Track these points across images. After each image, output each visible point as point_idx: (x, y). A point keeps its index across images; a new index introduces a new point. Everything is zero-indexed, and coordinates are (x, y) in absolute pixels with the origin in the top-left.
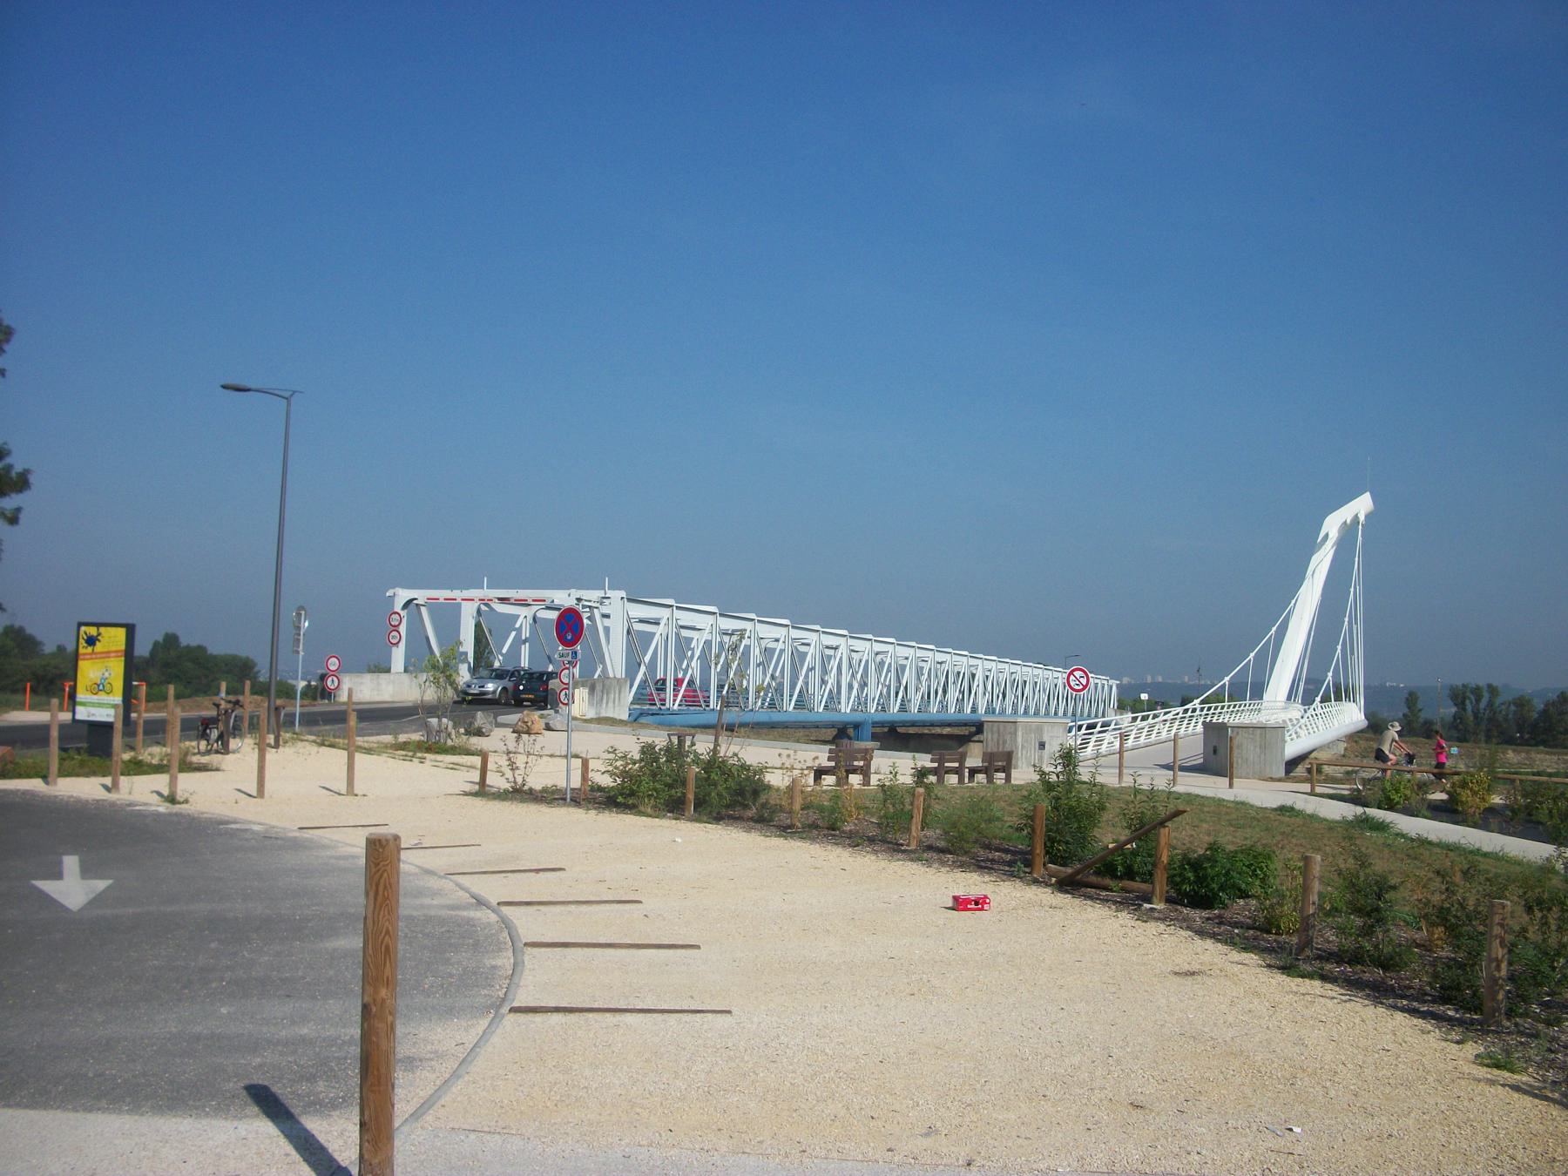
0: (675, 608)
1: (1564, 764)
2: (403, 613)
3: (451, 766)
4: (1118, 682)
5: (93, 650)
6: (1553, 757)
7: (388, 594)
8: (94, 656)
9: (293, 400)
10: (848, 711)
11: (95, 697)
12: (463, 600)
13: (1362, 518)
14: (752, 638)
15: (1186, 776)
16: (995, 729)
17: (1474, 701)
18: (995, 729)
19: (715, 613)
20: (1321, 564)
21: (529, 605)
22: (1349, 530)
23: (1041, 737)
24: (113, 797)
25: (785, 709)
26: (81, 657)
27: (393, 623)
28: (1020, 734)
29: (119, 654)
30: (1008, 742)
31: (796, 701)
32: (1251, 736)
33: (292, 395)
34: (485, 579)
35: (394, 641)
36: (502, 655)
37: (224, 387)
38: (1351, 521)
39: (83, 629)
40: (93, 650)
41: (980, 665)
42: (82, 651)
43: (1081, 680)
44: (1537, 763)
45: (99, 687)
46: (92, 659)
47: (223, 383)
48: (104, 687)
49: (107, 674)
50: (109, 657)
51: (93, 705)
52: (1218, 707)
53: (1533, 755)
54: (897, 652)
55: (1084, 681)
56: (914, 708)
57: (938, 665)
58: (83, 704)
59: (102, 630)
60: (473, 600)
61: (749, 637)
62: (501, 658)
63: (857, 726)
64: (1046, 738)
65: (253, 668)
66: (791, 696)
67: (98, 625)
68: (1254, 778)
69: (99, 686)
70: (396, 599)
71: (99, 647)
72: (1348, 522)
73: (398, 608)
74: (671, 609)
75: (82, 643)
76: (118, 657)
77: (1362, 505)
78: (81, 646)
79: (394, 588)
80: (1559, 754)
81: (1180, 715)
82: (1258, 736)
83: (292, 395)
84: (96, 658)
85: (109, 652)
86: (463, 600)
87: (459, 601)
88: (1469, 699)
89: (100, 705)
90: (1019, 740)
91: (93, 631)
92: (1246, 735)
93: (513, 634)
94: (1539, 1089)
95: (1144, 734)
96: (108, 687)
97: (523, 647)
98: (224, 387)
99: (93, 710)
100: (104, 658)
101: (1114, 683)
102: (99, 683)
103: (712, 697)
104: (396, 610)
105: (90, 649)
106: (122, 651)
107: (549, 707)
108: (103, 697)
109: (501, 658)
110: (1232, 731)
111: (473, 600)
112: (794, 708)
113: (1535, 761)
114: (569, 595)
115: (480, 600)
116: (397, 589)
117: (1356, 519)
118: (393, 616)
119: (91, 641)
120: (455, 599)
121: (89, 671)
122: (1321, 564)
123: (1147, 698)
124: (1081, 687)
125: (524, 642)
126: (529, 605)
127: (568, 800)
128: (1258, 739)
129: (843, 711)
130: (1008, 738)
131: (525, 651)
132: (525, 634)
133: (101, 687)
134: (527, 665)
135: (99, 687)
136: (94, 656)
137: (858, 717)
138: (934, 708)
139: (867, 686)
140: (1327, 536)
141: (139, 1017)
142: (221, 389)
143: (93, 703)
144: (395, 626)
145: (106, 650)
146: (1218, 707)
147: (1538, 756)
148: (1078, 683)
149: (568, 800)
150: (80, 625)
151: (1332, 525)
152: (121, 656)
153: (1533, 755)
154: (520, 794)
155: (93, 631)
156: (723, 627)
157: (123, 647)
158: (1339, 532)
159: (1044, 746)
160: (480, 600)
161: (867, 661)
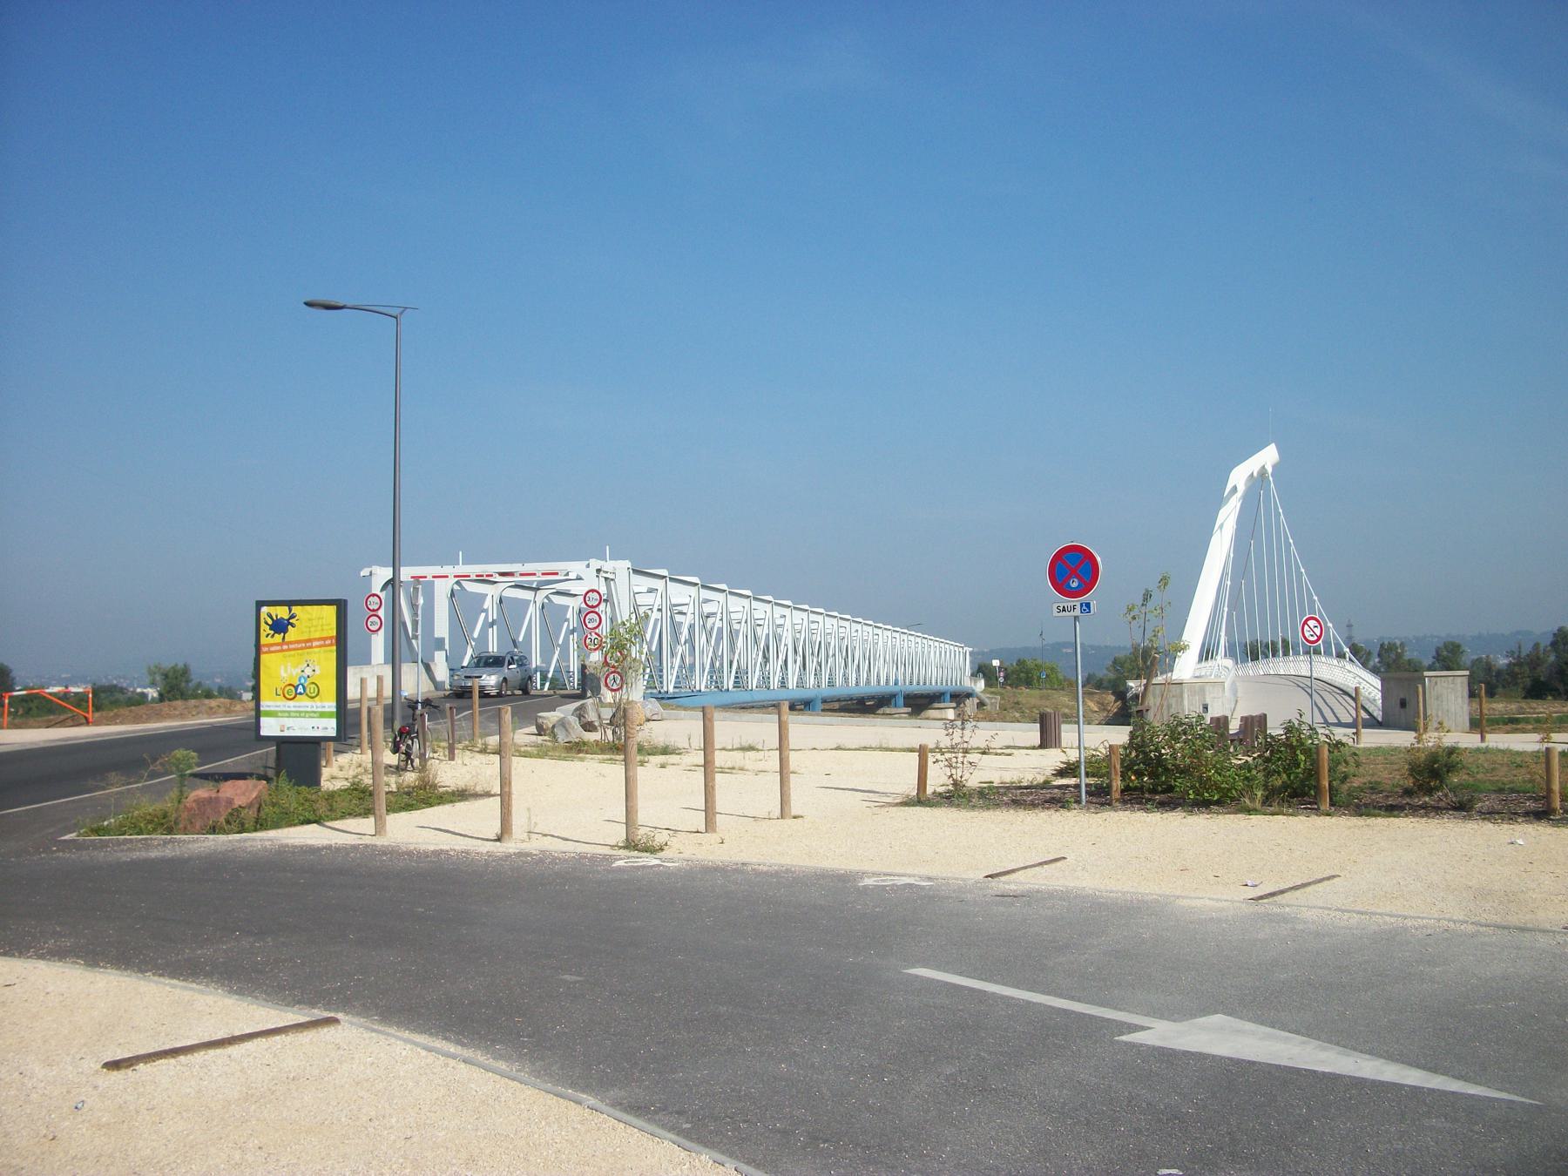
0: (668, 579)
2: (382, 595)
3: (693, 768)
4: (971, 649)
5: (284, 638)
7: (362, 574)
8: (285, 646)
9: (403, 319)
11: (291, 703)
12: (434, 577)
13: (1270, 470)
14: (664, 610)
15: (1381, 733)
16: (1158, 692)
18: (1158, 692)
19: (696, 584)
20: (1228, 516)
21: (496, 582)
22: (1258, 481)
23: (1204, 698)
24: (379, 841)
25: (750, 688)
26: (264, 649)
27: (371, 607)
28: (1186, 695)
29: (328, 642)
30: (1174, 706)
32: (1452, 686)
33: (401, 313)
34: (461, 553)
35: (372, 628)
36: (474, 639)
37: (308, 304)
38: (1258, 473)
39: (265, 610)
40: (284, 638)
41: (898, 637)
42: (264, 640)
43: (1315, 630)
45: (295, 690)
46: (282, 651)
47: (308, 299)
48: (304, 688)
49: (308, 671)
50: (311, 647)
51: (289, 714)
54: (828, 626)
55: (1318, 631)
58: (270, 714)
59: (296, 610)
60: (447, 577)
61: (660, 610)
62: (473, 644)
63: (943, 694)
64: (1208, 701)
65: (8, 675)
67: (290, 604)
68: (1457, 731)
69: (296, 688)
70: (373, 578)
71: (292, 634)
72: (1255, 474)
73: (376, 589)
75: (265, 629)
76: (325, 646)
77: (1268, 457)
78: (263, 635)
79: (371, 567)
82: (1459, 685)
83: (401, 313)
84: (289, 650)
85: (310, 640)
86: (434, 577)
87: (430, 578)
89: (300, 714)
90: (1186, 702)
91: (282, 612)
92: (1445, 685)
93: (483, 615)
96: (311, 689)
97: (490, 630)
98: (308, 304)
99: (288, 722)
100: (302, 648)
101: (969, 650)
102: (296, 683)
104: (374, 592)
105: (278, 638)
106: (331, 638)
107: (589, 694)
108: (303, 703)
109: (473, 644)
110: (1430, 681)
111: (447, 577)
114: (588, 566)
115: (455, 576)
116: (374, 567)
117: (1263, 471)
118: (371, 599)
119: (280, 627)
120: (425, 577)
121: (278, 668)
122: (1228, 516)
124: (1315, 638)
125: (492, 625)
126: (496, 582)
127: (1116, 795)
128: (1460, 689)
130: (1173, 701)
131: (493, 634)
132: (493, 615)
133: (300, 689)
134: (495, 650)
135: (295, 690)
136: (285, 647)
137: (896, 689)
140: (1235, 489)
141: (93, 1126)
142: (305, 306)
143: (289, 712)
144: (374, 610)
145: (305, 637)
148: (1312, 633)
149: (1116, 795)
150: (260, 604)
151: (1239, 476)
152: (331, 645)
154: (956, 796)
155: (282, 612)
157: (334, 633)
158: (1246, 484)
159: (1207, 708)
160: (455, 576)
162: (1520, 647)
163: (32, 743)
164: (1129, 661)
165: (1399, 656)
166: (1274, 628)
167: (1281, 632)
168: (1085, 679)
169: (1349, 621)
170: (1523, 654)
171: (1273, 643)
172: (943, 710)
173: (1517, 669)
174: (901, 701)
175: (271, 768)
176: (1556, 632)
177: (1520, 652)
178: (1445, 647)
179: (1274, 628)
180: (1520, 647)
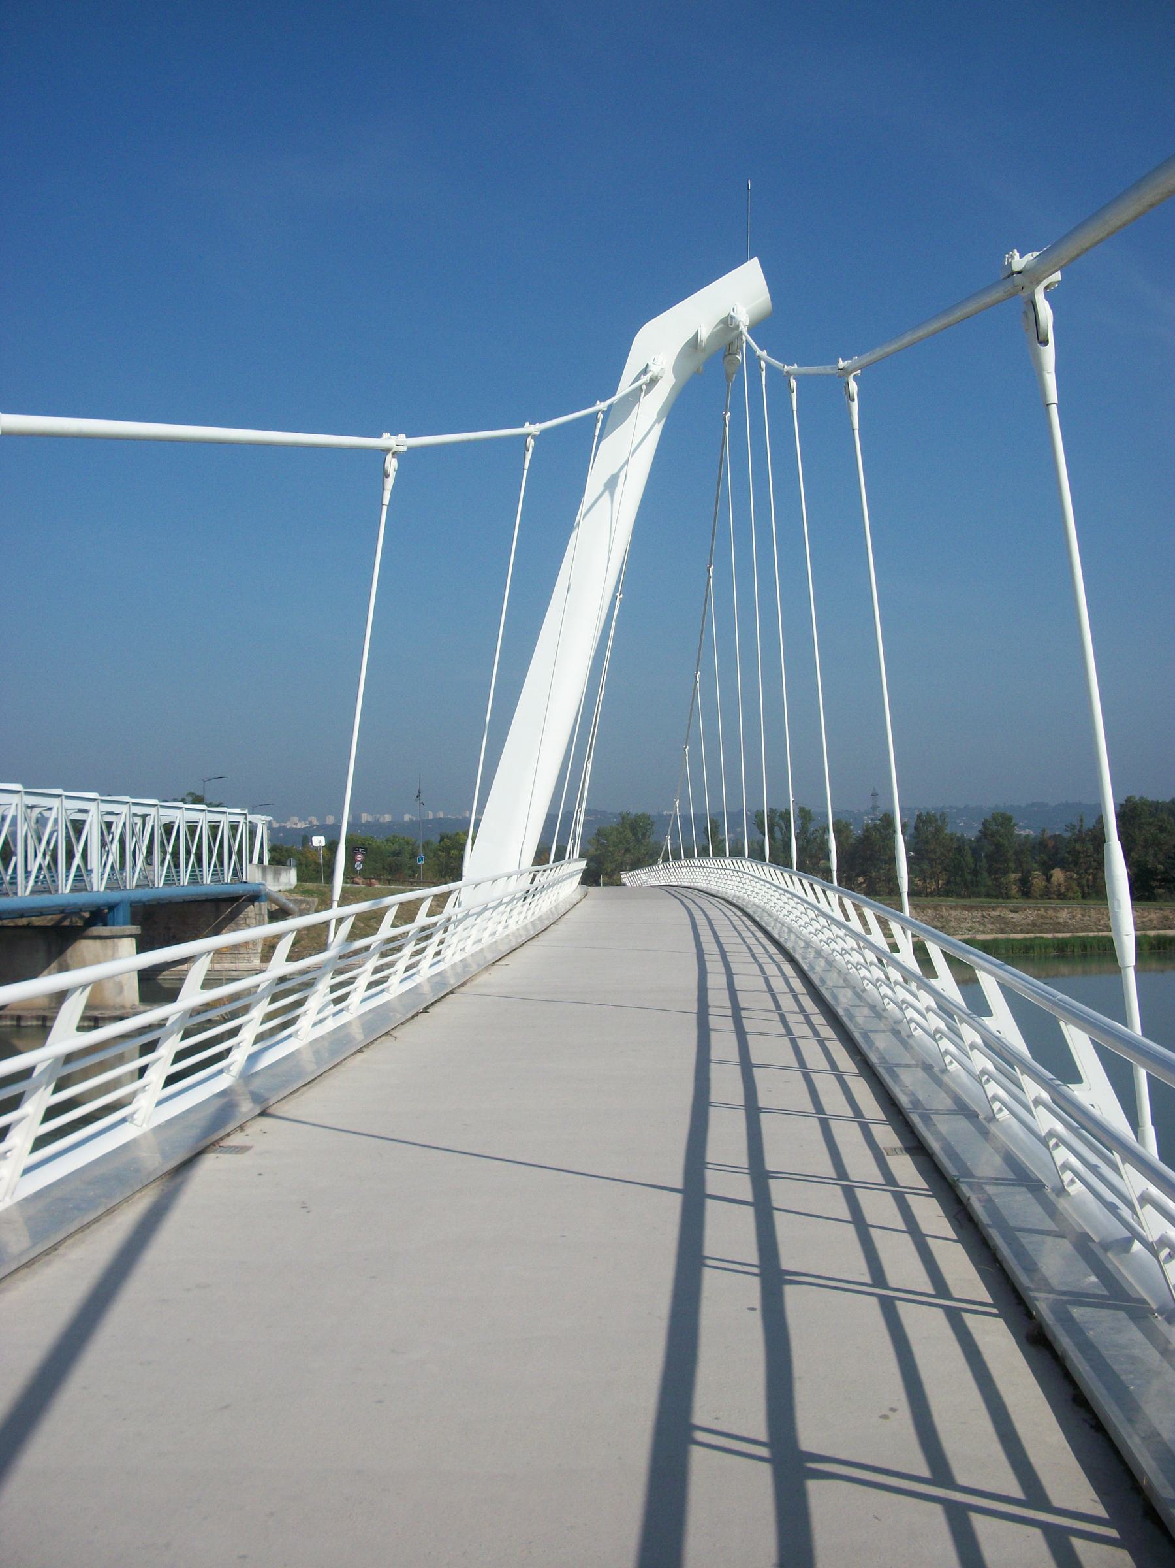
1: (992, 923)
6: (975, 913)
10: (102, 889)
17: (784, 828)
31: (75, 876)
44: (953, 924)
52: (415, 905)
53: (945, 913)
56: (98, 884)
57: (29, 811)
63: (112, 907)
66: (187, 867)
74: (60, 798)
80: (983, 908)
81: (279, 966)
88: (779, 825)
94: (1108, 1298)
95: (362, 982)
101: (261, 821)
103: (204, 871)
112: (164, 884)
113: (948, 921)
123: (323, 844)
129: (95, 889)
137: (115, 896)
138: (65, 886)
139: (16, 855)
146: (415, 905)
147: (954, 913)
153: (945, 913)
156: (27, 803)
161: (14, 819)
162: (1081, 820)
163: (923, 1136)
164: (615, 833)
165: (939, 830)
166: (734, 795)
167: (679, 812)
168: (911, 830)
169: (874, 789)
170: (1085, 828)
171: (805, 815)
172: (108, 941)
173: (1078, 847)
174: (123, 913)
175: (722, 1105)
176: (1124, 802)
177: (1081, 826)
178: (994, 819)
179: (734, 795)
180: (1081, 820)
